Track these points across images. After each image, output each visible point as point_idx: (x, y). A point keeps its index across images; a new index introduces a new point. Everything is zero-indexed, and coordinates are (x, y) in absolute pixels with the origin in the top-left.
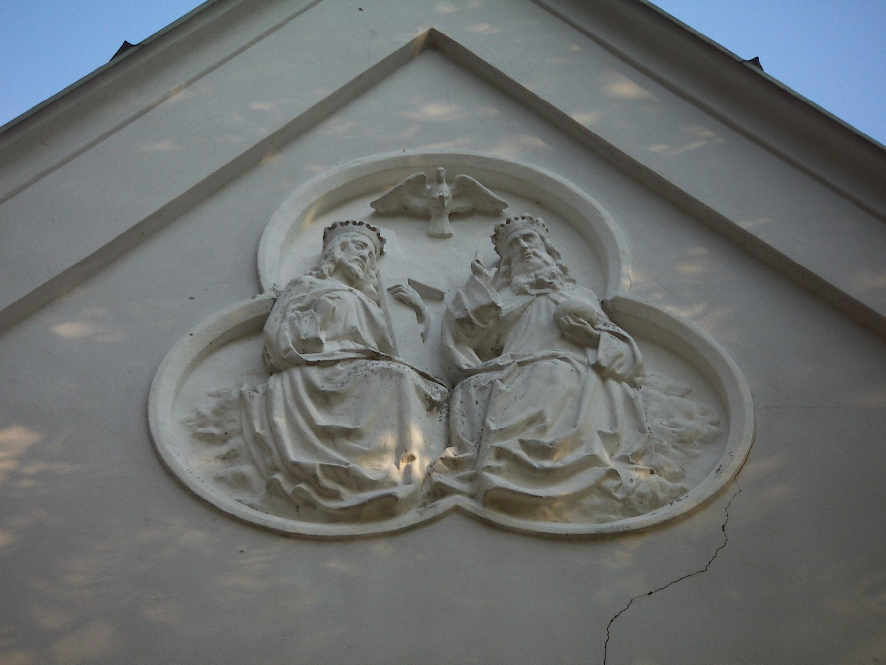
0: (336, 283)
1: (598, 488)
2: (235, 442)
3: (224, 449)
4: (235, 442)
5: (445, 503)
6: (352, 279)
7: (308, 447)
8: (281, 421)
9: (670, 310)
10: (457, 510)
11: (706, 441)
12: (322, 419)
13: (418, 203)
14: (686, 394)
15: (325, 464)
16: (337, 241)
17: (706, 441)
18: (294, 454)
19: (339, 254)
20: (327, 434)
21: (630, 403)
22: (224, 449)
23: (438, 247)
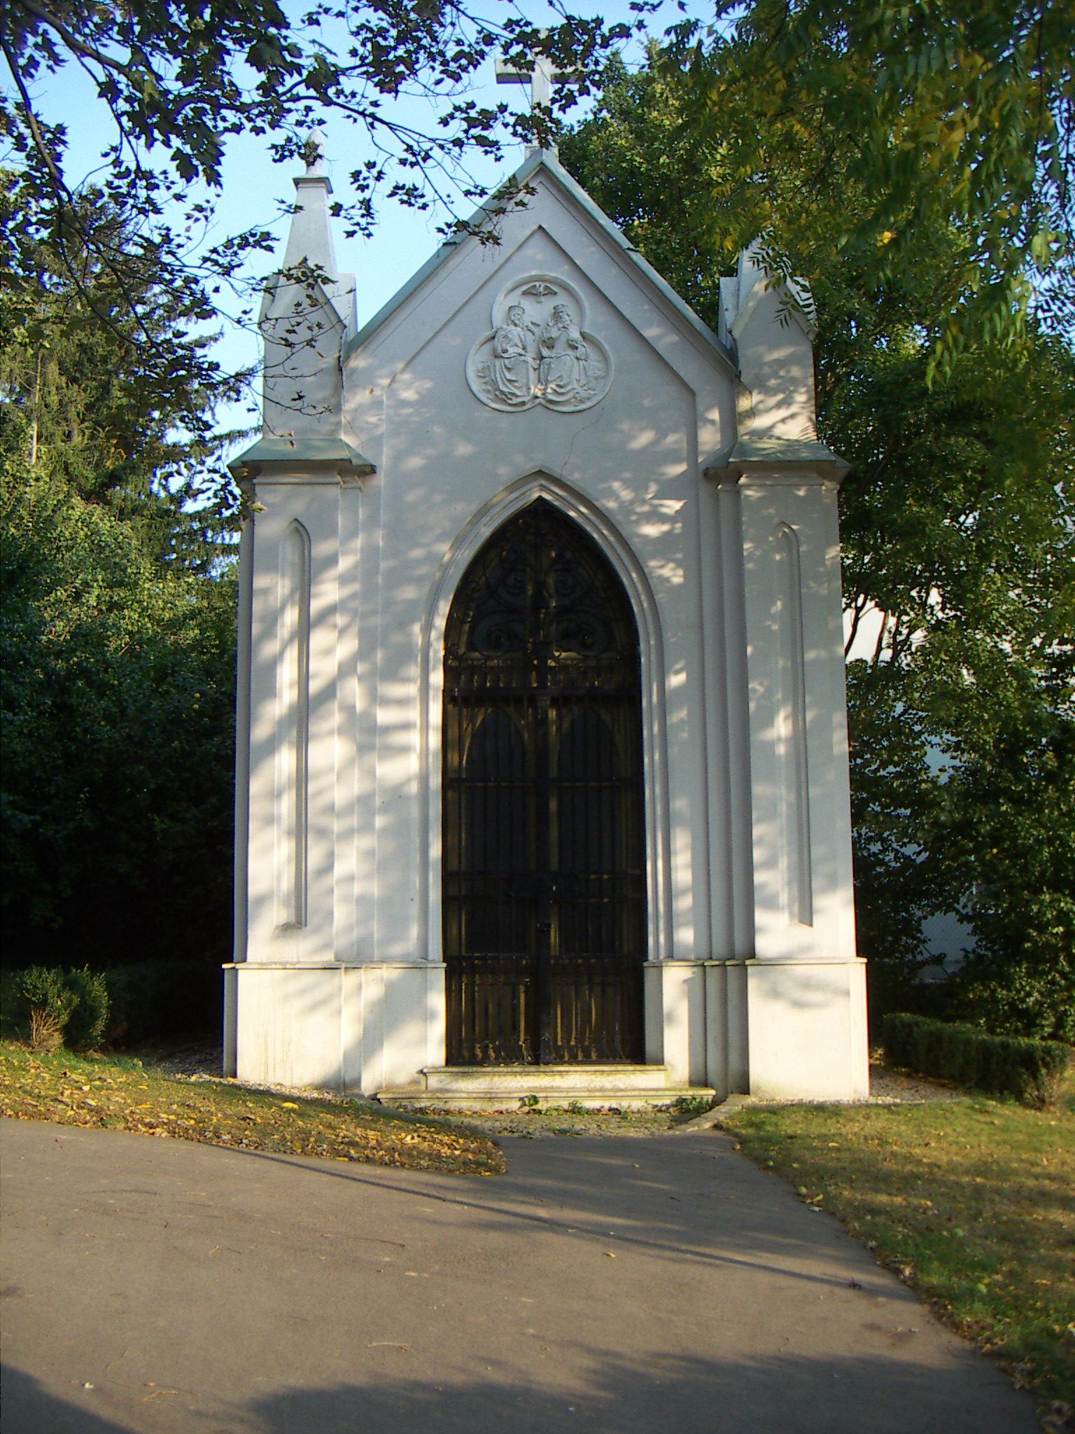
0: (512, 327)
1: (575, 397)
2: (487, 379)
3: (484, 380)
4: (487, 379)
5: (537, 401)
6: (516, 325)
7: (507, 387)
8: (498, 376)
9: (418, 886)
10: (540, 404)
11: (603, 378)
12: (509, 377)
13: (534, 292)
14: (599, 361)
15: (557, 1064)
16: (513, 312)
17: (603, 378)
18: (502, 388)
19: (513, 318)
20: (510, 381)
21: (584, 367)
22: (484, 380)
23: (539, 305)
